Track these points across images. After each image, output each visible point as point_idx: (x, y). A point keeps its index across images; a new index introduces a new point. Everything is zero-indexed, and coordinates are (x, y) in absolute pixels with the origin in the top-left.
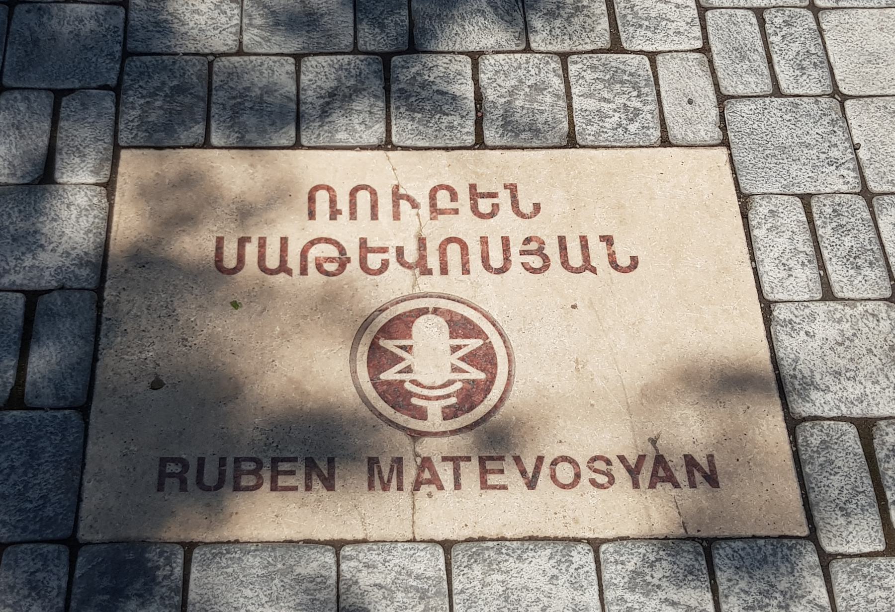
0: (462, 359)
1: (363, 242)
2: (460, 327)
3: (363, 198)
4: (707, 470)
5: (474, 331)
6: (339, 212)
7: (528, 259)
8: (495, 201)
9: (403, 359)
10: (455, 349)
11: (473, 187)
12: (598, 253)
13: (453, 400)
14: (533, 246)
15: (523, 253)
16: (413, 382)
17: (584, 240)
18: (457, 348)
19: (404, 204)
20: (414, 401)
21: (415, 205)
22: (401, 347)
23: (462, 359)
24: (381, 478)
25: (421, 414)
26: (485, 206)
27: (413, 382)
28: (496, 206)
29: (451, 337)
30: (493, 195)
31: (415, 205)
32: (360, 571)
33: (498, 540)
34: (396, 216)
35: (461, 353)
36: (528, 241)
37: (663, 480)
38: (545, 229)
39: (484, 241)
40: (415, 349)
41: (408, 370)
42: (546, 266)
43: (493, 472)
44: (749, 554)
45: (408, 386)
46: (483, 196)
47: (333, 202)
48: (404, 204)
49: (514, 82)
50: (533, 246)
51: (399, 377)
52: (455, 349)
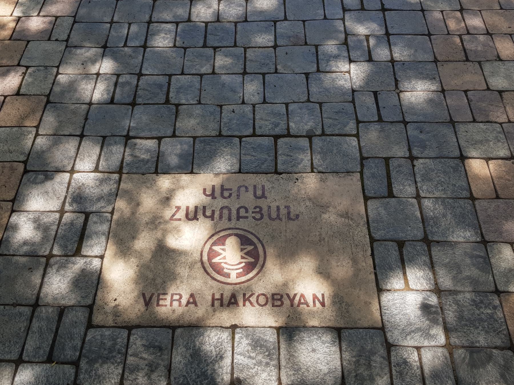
0: (222, 254)
4: (147, 300)
5: (251, 243)
7: (253, 215)
8: (230, 192)
9: (222, 254)
13: (241, 270)
14: (258, 210)
15: (253, 213)
16: (226, 263)
18: (223, 250)
20: (225, 270)
24: (319, 300)
25: (228, 276)
26: (226, 194)
27: (226, 263)
28: (230, 195)
30: (231, 190)
32: (242, 338)
33: (368, 328)
35: (245, 251)
36: (255, 208)
37: (192, 303)
42: (262, 218)
43: (162, 299)
44: (355, 335)
45: (223, 264)
46: (227, 190)
47: (230, 214)
50: (258, 210)
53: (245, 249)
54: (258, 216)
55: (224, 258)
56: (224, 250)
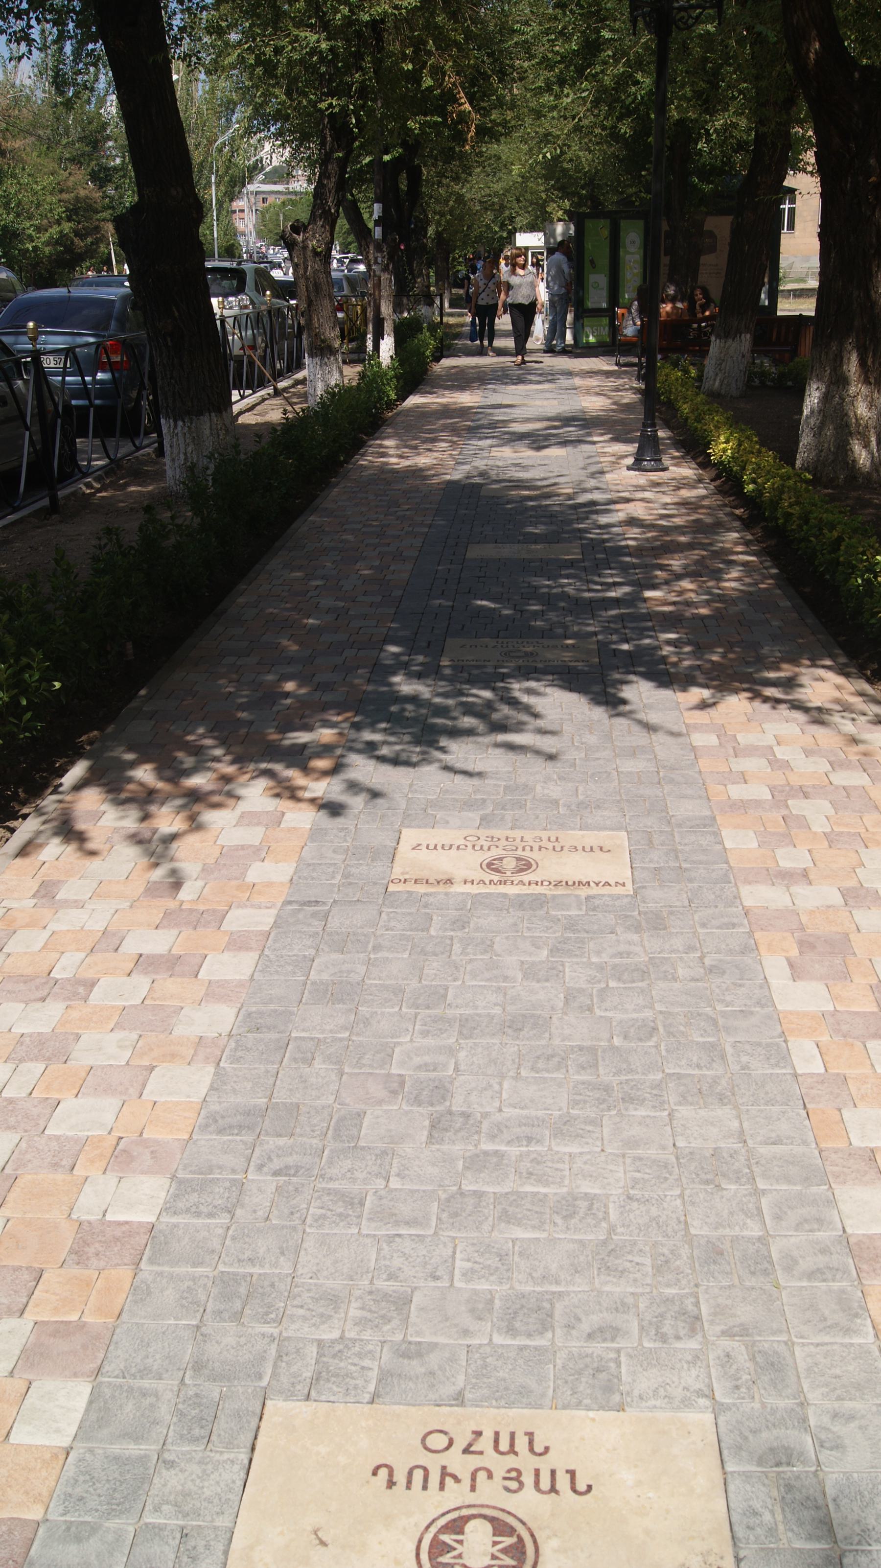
0: (455, 1549)
1: (444, 1468)
2: (500, 1527)
3: (418, 1475)
5: (511, 1531)
6: (394, 1484)
7: (509, 1483)
10: (495, 1543)
11: (444, 1468)
12: (563, 1482)
15: (505, 1478)
17: (553, 1473)
19: (448, 1480)
21: (457, 1480)
22: (500, 1542)
23: (455, 1549)
29: (494, 1535)
31: (457, 1480)
34: (442, 1486)
35: (500, 1546)
36: (509, 1471)
38: (557, 1460)
39: (537, 1472)
40: (465, 1543)
41: (460, 1556)
48: (448, 1480)
49: (582, 1366)
50: (514, 1474)
51: (452, 1561)
52: (495, 1543)
53: (500, 1542)
54: (514, 1485)
55: (460, 1556)
56: (461, 1542)
